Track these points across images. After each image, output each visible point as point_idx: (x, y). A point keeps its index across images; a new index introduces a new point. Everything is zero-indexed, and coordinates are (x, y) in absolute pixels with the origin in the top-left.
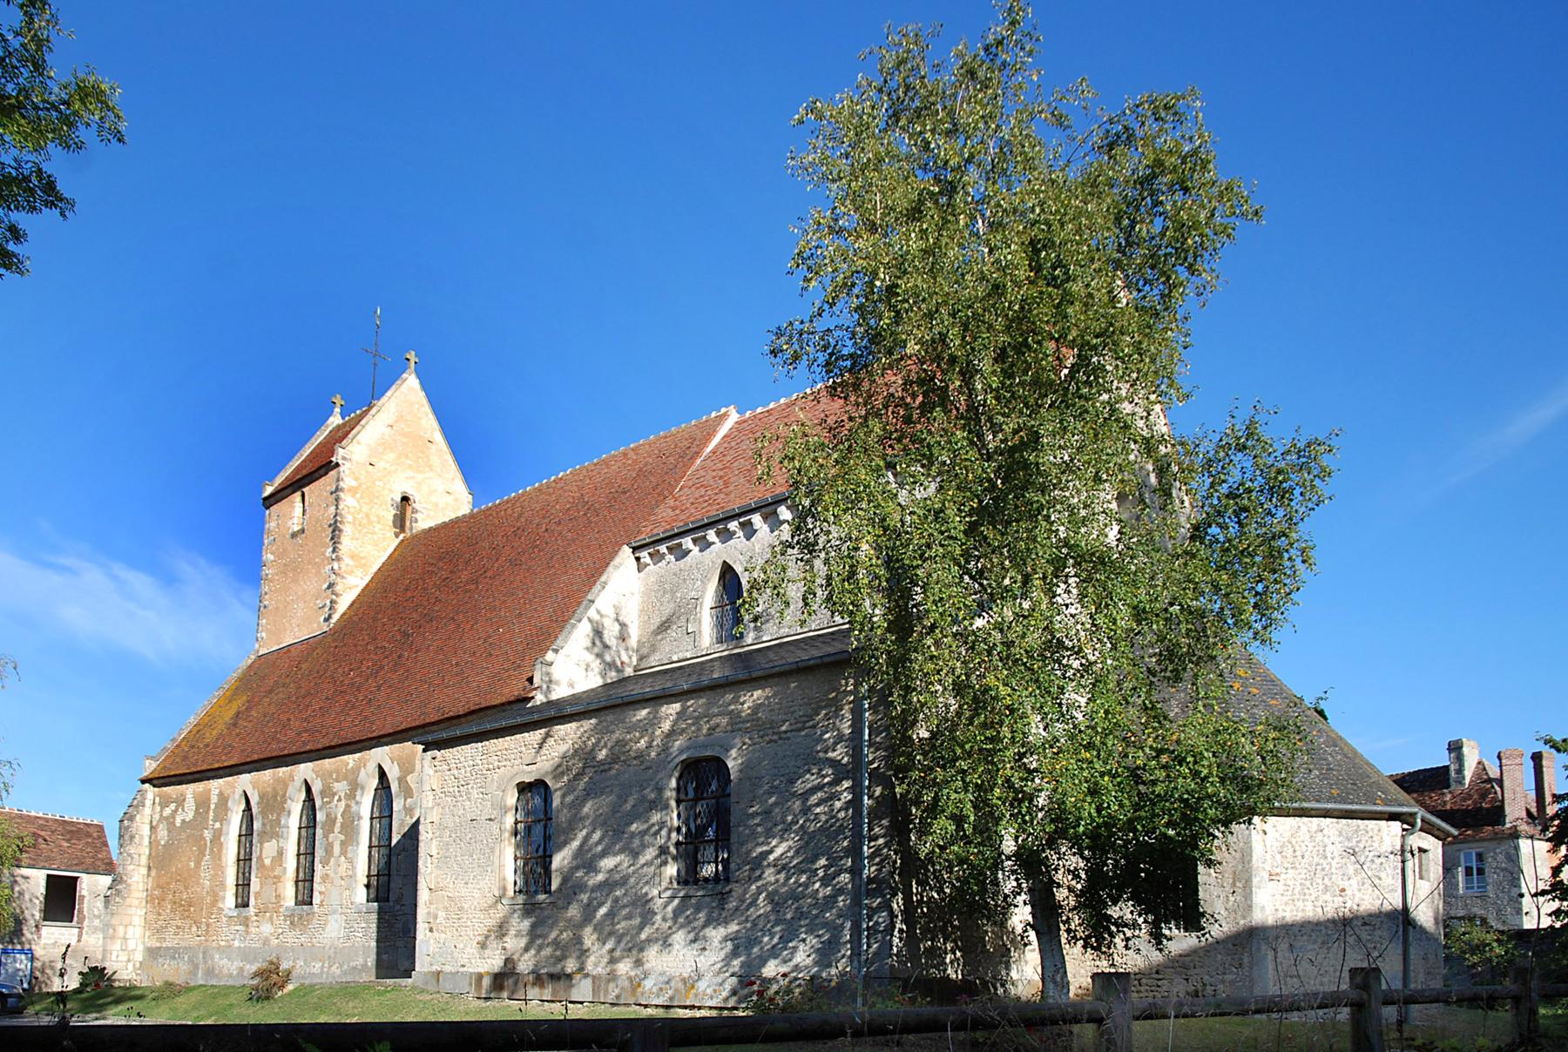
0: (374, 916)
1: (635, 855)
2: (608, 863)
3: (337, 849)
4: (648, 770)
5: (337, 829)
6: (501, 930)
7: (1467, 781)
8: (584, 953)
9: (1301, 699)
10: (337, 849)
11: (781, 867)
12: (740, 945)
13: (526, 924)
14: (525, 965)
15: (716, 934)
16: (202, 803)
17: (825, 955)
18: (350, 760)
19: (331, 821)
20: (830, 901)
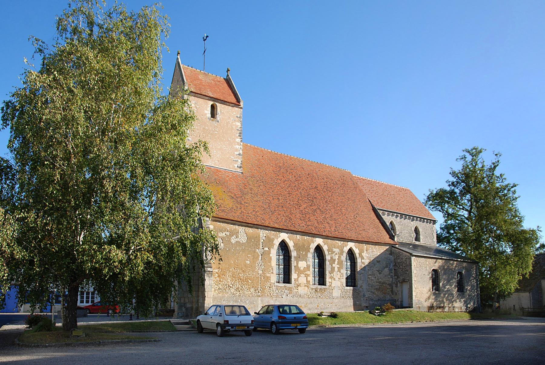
0: (352, 291)
1: (451, 286)
2: (447, 287)
3: (336, 269)
4: (453, 271)
5: (336, 262)
6: (429, 298)
7: (12, 162)
8: (444, 303)
9: (7, 104)
10: (336, 269)
11: (469, 290)
12: (465, 302)
13: (434, 297)
14: (435, 305)
15: (462, 300)
16: (253, 241)
17: (474, 304)
18: (340, 243)
19: (333, 261)
20: (474, 296)
